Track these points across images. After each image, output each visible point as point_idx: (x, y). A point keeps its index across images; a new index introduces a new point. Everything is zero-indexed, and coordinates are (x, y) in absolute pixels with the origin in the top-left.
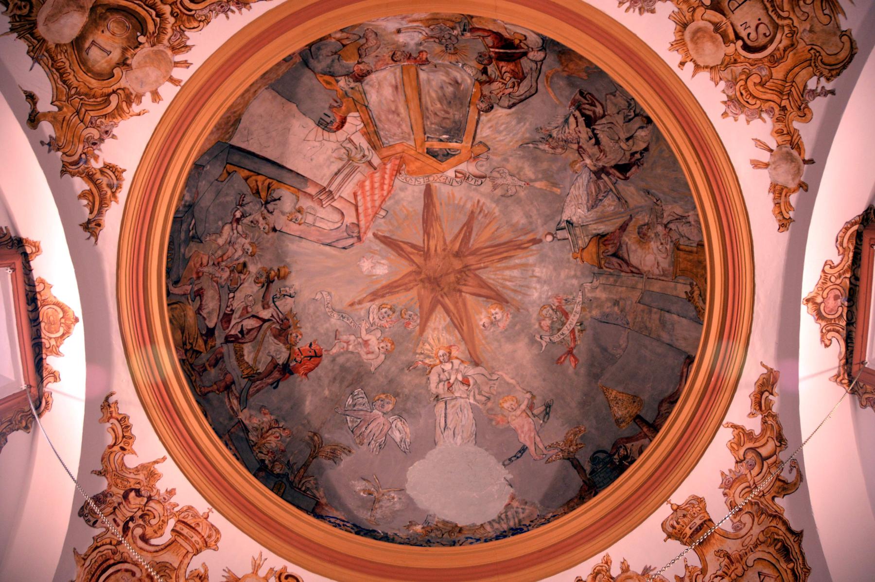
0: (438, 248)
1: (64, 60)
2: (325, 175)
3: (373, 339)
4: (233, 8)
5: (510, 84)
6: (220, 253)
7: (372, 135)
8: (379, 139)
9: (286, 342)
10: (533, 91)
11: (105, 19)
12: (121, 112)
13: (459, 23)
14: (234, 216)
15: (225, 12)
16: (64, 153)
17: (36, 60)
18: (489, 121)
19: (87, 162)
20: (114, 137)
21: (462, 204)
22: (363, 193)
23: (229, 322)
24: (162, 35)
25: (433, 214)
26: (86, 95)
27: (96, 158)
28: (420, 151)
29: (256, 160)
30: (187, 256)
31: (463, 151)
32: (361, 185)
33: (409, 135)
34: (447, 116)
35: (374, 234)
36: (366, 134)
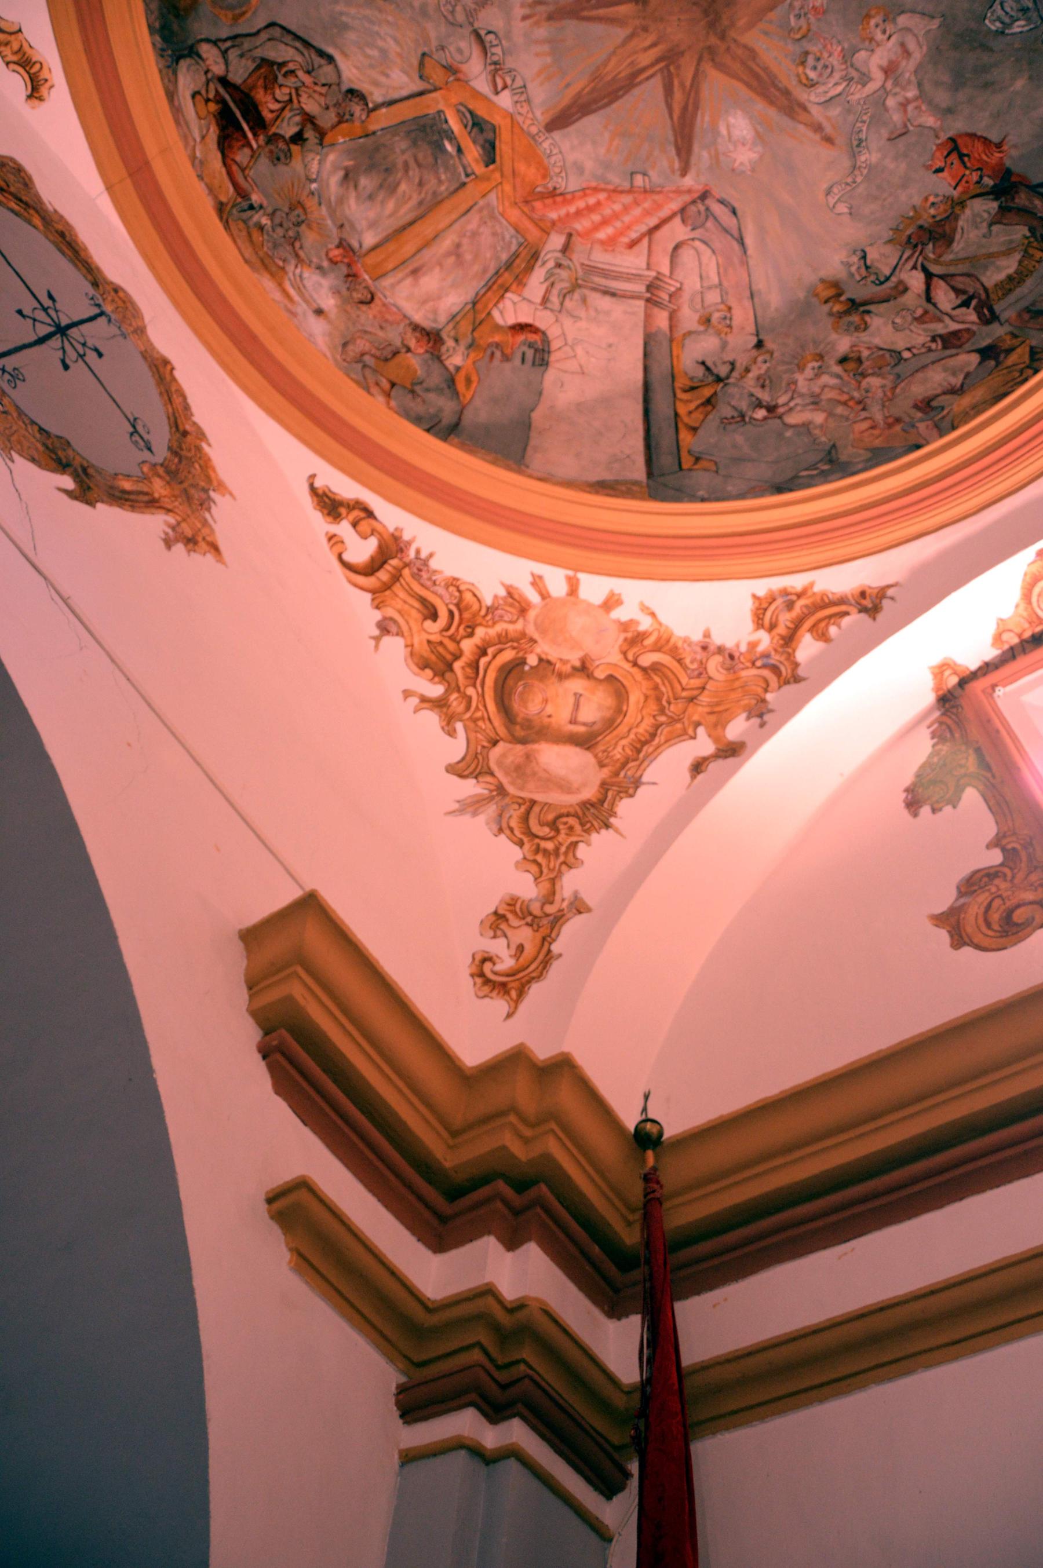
0: (648, 43)
1: (619, 749)
2: (625, 312)
3: (875, 61)
4: (412, 554)
5: (291, 81)
6: (840, 410)
7: (517, 271)
8: (516, 255)
9: (952, 217)
10: (277, 32)
11: (529, 720)
12: (663, 642)
13: (244, 222)
14: (765, 419)
15: (425, 562)
16: (766, 691)
17: (637, 783)
18: (376, 84)
19: (766, 655)
20: (707, 634)
21: (546, 48)
22: (622, 233)
23: (955, 334)
24: (512, 635)
25: (593, 90)
26: (659, 699)
27: (753, 645)
28: (497, 175)
29: (654, 430)
30: (869, 455)
31: (454, 100)
32: (609, 244)
33: (481, 210)
34: (412, 163)
35: (684, 172)
36: (520, 281)
